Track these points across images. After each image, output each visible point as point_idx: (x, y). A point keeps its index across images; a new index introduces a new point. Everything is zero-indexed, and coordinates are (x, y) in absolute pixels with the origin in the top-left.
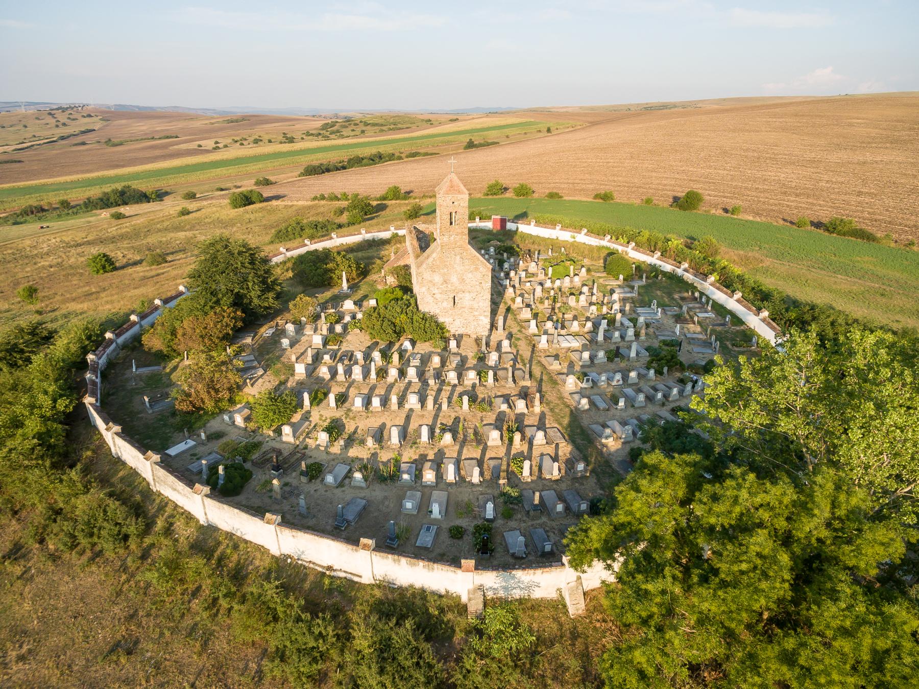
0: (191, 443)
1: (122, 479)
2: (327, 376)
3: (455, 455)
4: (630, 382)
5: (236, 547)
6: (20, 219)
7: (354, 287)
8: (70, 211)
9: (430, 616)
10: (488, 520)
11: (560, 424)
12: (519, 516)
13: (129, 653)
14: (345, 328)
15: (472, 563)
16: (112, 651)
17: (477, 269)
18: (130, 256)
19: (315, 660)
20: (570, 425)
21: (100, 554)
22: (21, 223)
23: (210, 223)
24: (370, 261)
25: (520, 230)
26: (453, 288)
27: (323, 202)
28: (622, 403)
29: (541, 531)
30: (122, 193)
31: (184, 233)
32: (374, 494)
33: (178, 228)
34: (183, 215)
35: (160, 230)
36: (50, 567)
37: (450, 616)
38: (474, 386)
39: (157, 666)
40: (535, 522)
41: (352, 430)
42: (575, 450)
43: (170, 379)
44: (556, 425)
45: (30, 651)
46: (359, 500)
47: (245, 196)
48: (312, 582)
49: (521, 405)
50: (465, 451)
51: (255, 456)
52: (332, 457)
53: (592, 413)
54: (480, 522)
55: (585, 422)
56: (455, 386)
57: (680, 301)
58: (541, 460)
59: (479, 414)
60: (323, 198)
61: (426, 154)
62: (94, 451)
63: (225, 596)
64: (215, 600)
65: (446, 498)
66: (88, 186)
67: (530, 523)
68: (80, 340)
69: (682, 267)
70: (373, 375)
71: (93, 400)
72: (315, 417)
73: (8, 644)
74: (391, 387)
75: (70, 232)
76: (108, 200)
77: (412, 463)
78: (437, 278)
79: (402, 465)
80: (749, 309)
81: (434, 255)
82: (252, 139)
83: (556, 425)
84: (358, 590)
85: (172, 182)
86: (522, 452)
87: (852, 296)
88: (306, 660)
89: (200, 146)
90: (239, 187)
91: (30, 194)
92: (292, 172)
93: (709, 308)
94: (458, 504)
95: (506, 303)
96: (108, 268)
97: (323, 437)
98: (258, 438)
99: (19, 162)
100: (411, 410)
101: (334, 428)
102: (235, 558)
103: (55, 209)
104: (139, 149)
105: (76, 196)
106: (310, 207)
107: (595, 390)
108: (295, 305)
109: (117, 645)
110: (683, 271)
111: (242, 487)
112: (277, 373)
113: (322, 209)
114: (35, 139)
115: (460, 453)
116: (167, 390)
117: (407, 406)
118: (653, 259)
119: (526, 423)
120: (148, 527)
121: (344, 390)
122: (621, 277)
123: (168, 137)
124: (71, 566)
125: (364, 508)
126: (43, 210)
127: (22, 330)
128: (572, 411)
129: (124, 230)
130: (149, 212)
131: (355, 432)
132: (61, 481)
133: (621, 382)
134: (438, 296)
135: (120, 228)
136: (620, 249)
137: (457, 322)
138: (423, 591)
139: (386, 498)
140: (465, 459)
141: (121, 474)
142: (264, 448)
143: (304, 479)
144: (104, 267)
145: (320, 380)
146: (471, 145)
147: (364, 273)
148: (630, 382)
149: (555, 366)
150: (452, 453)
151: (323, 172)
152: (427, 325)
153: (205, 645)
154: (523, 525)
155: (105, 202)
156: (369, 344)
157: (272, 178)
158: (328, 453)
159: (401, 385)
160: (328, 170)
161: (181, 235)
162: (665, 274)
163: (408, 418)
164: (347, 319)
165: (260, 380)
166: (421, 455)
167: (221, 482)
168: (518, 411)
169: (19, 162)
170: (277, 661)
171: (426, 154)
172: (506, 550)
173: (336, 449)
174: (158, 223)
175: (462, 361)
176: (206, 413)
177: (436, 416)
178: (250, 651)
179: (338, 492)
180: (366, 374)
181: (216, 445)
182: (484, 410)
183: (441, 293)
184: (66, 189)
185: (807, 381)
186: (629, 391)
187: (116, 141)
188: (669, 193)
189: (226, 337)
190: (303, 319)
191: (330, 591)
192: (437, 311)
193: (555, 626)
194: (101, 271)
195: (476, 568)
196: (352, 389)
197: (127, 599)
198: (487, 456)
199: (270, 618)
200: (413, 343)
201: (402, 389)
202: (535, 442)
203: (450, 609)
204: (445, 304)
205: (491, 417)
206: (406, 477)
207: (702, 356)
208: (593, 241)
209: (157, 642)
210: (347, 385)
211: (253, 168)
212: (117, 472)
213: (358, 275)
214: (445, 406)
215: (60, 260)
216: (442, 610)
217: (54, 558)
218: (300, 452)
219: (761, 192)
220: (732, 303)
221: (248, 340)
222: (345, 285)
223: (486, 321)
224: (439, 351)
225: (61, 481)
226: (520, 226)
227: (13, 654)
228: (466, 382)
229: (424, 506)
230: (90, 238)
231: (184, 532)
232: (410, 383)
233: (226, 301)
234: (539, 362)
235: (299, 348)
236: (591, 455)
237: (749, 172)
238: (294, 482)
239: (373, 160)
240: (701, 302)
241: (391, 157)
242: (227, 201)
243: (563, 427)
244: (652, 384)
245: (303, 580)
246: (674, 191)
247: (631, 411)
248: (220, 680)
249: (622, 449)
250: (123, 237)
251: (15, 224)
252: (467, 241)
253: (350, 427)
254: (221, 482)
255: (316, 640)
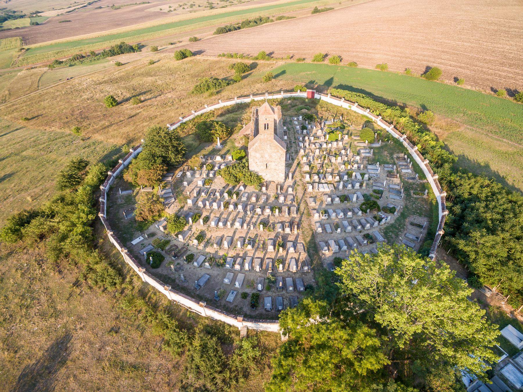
0: (142, 238)
1: (114, 254)
2: (202, 206)
3: (252, 255)
4: (348, 217)
5: (155, 294)
6: (73, 63)
7: (224, 143)
8: (96, 58)
9: (225, 335)
10: (259, 291)
11: (305, 241)
12: (273, 289)
13: (116, 332)
14: (214, 175)
15: (241, 319)
16: (110, 331)
17: (278, 151)
18: (124, 94)
19: (179, 347)
20: (310, 242)
21: (106, 289)
22: (73, 65)
23: (164, 70)
24: (233, 127)
25: (322, 99)
27: (224, 59)
28: (339, 230)
29: (281, 298)
30: (120, 47)
31: (150, 78)
32: (214, 272)
33: (148, 74)
34: (151, 64)
35: (139, 75)
36: (89, 291)
37: (233, 335)
38: (269, 216)
39: (126, 339)
40: (279, 293)
41: (209, 237)
42: (308, 258)
43: (135, 200)
44: (303, 242)
45: (84, 326)
46: (207, 275)
47: (182, 53)
48: (183, 313)
49: (288, 230)
50: (257, 253)
51: (167, 248)
52: (199, 251)
53: (323, 234)
54: (254, 291)
55: (318, 240)
56: (260, 215)
57: (396, 160)
58: (291, 261)
59: (268, 233)
60: (224, 55)
61: (288, 18)
62: (104, 239)
63: (150, 316)
64: (146, 316)
65: (243, 278)
66: (103, 41)
67: (277, 294)
68: (98, 176)
69: (403, 137)
70: (222, 207)
71: (102, 215)
72: (194, 229)
73: (77, 322)
74: (230, 213)
75: (96, 74)
76: (114, 51)
77: (232, 258)
79: (228, 259)
80: (430, 172)
81: (256, 144)
82: (189, 4)
83: (303, 242)
84: (200, 318)
85: (146, 38)
86: (283, 256)
87: (505, 156)
88: (176, 347)
89: (161, 10)
90: (181, 42)
91: (76, 46)
92: (210, 31)
93: (410, 166)
94: (248, 281)
95: (298, 159)
96: (115, 104)
97: (195, 242)
98: (169, 238)
99: (69, 21)
100: (237, 229)
101: (201, 237)
102: (155, 298)
103: (89, 56)
104: (129, 12)
105: (99, 48)
106: (216, 62)
107: (329, 221)
108: (191, 162)
109: (112, 329)
110: (402, 139)
111: (160, 265)
112: (180, 201)
113: (223, 64)
114: (77, 4)
115: (254, 254)
116: (133, 206)
117: (235, 227)
118: (390, 129)
119: (288, 239)
120: (124, 279)
121: (208, 214)
122: (367, 142)
123: (144, 3)
124: (96, 293)
125: (208, 279)
126: (83, 57)
127: (74, 163)
128: (313, 233)
129: (122, 74)
130: (134, 61)
131: (210, 238)
132: (91, 256)
133: (343, 217)
134: (258, 163)
135: (120, 73)
136: (374, 119)
137: (268, 176)
138: (225, 323)
139: (218, 275)
140: (256, 258)
141: (114, 252)
142: (172, 244)
143: (185, 263)
144: (112, 104)
145: (198, 208)
146: (316, 11)
147: (230, 133)
148: (348, 217)
149: (312, 204)
150: (250, 254)
151: (227, 32)
152: (252, 178)
153: (142, 333)
154: (274, 294)
155: (112, 53)
156: (224, 185)
157: (198, 36)
158: (197, 249)
159: (235, 213)
160: (230, 30)
161: (150, 79)
162: (394, 139)
163: (235, 233)
164: (216, 168)
165: (173, 205)
166: (237, 254)
167: (151, 263)
168: (286, 232)
169: (69, 21)
170: (166, 345)
171: (288, 18)
172: (264, 306)
173: (201, 247)
174: (139, 69)
175: (267, 198)
176: (148, 222)
177: (248, 233)
178: (158, 338)
179: (199, 269)
180: (219, 207)
181: (152, 240)
182: (270, 231)
184: (93, 43)
186: (345, 223)
187: (117, 5)
188: (425, 63)
189: (159, 180)
190: (196, 168)
191: (189, 318)
193: (274, 344)
194: (111, 106)
195: (243, 320)
196: (212, 214)
197: (116, 311)
198: (266, 257)
199: (165, 327)
200: (245, 186)
201: (235, 215)
202: (289, 252)
203: (233, 332)
204: (262, 167)
205: (273, 235)
206: (228, 266)
207: (393, 201)
208: (360, 111)
209: (126, 329)
210: (210, 211)
211: (188, 28)
212: (112, 251)
213: (227, 136)
214: (252, 228)
215: (92, 95)
216: (230, 332)
217: (90, 288)
218: (186, 247)
219: (486, 63)
220: (423, 165)
221: (170, 179)
222: (219, 144)
223: (283, 176)
224: (257, 191)
225: (91, 256)
226: (322, 96)
227: (78, 326)
228: (265, 214)
229: (233, 281)
230: (106, 79)
231: (137, 284)
232: (239, 212)
233: (159, 161)
234: (305, 201)
235: (192, 186)
236: (315, 259)
237: (485, 44)
238: (182, 263)
239: (256, 23)
240: (407, 162)
241: (268, 20)
242: (173, 55)
243: (306, 243)
244: (360, 218)
245: (180, 311)
246: (428, 61)
247: (343, 234)
248: (147, 348)
249: (332, 256)
250: (121, 79)
251: (71, 66)
253: (208, 236)
254: (151, 263)
255: (180, 340)
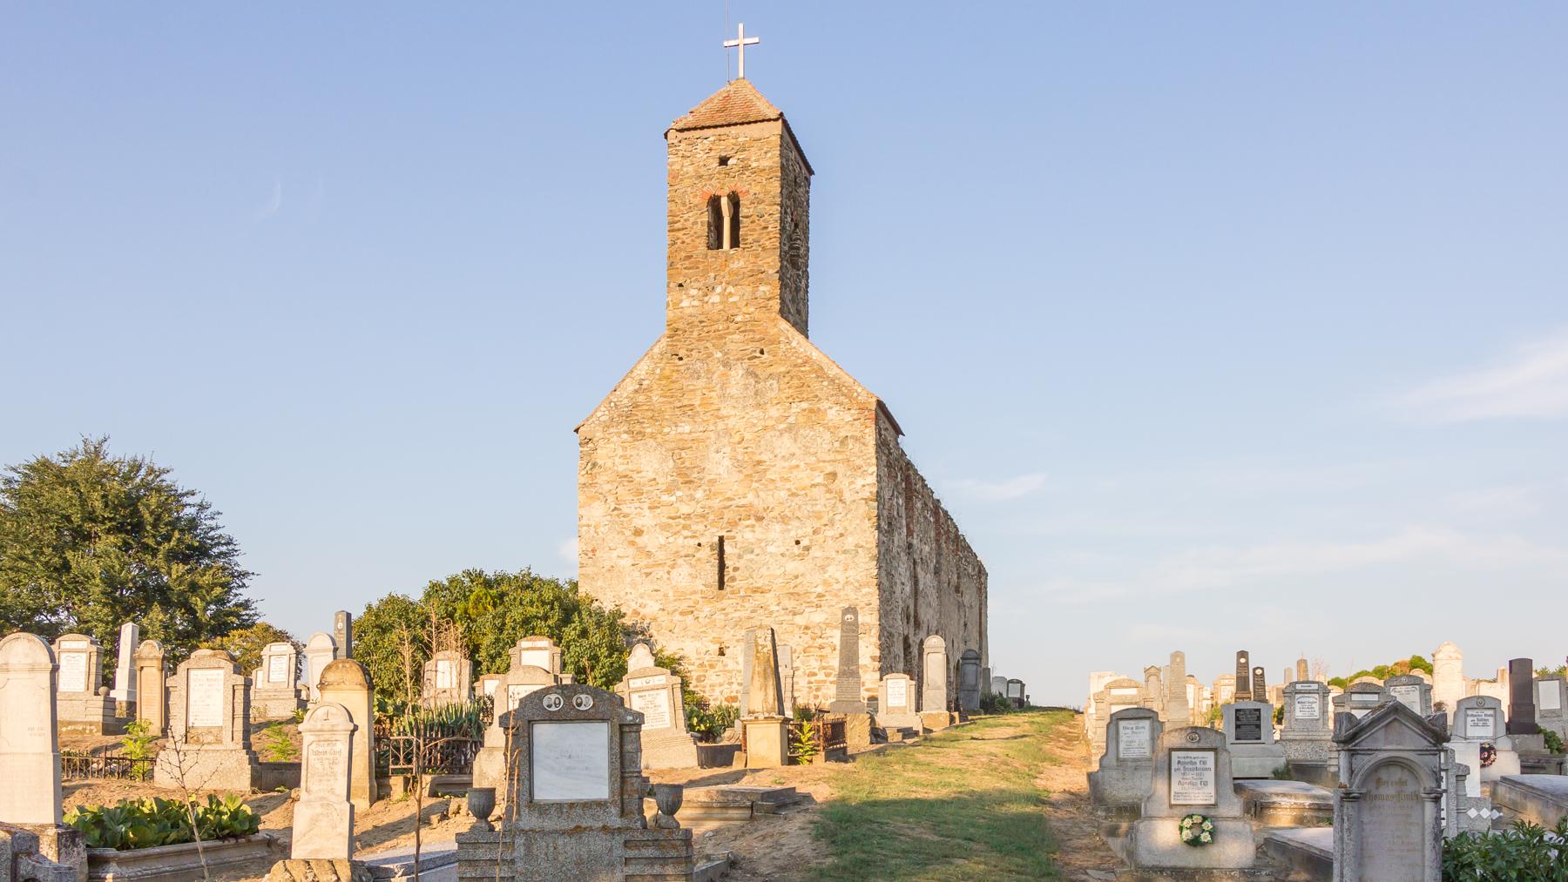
26: (716, 503)
78: (651, 463)
183: (664, 527)
185: (205, 575)
192: (652, 608)
252: (776, 305)
